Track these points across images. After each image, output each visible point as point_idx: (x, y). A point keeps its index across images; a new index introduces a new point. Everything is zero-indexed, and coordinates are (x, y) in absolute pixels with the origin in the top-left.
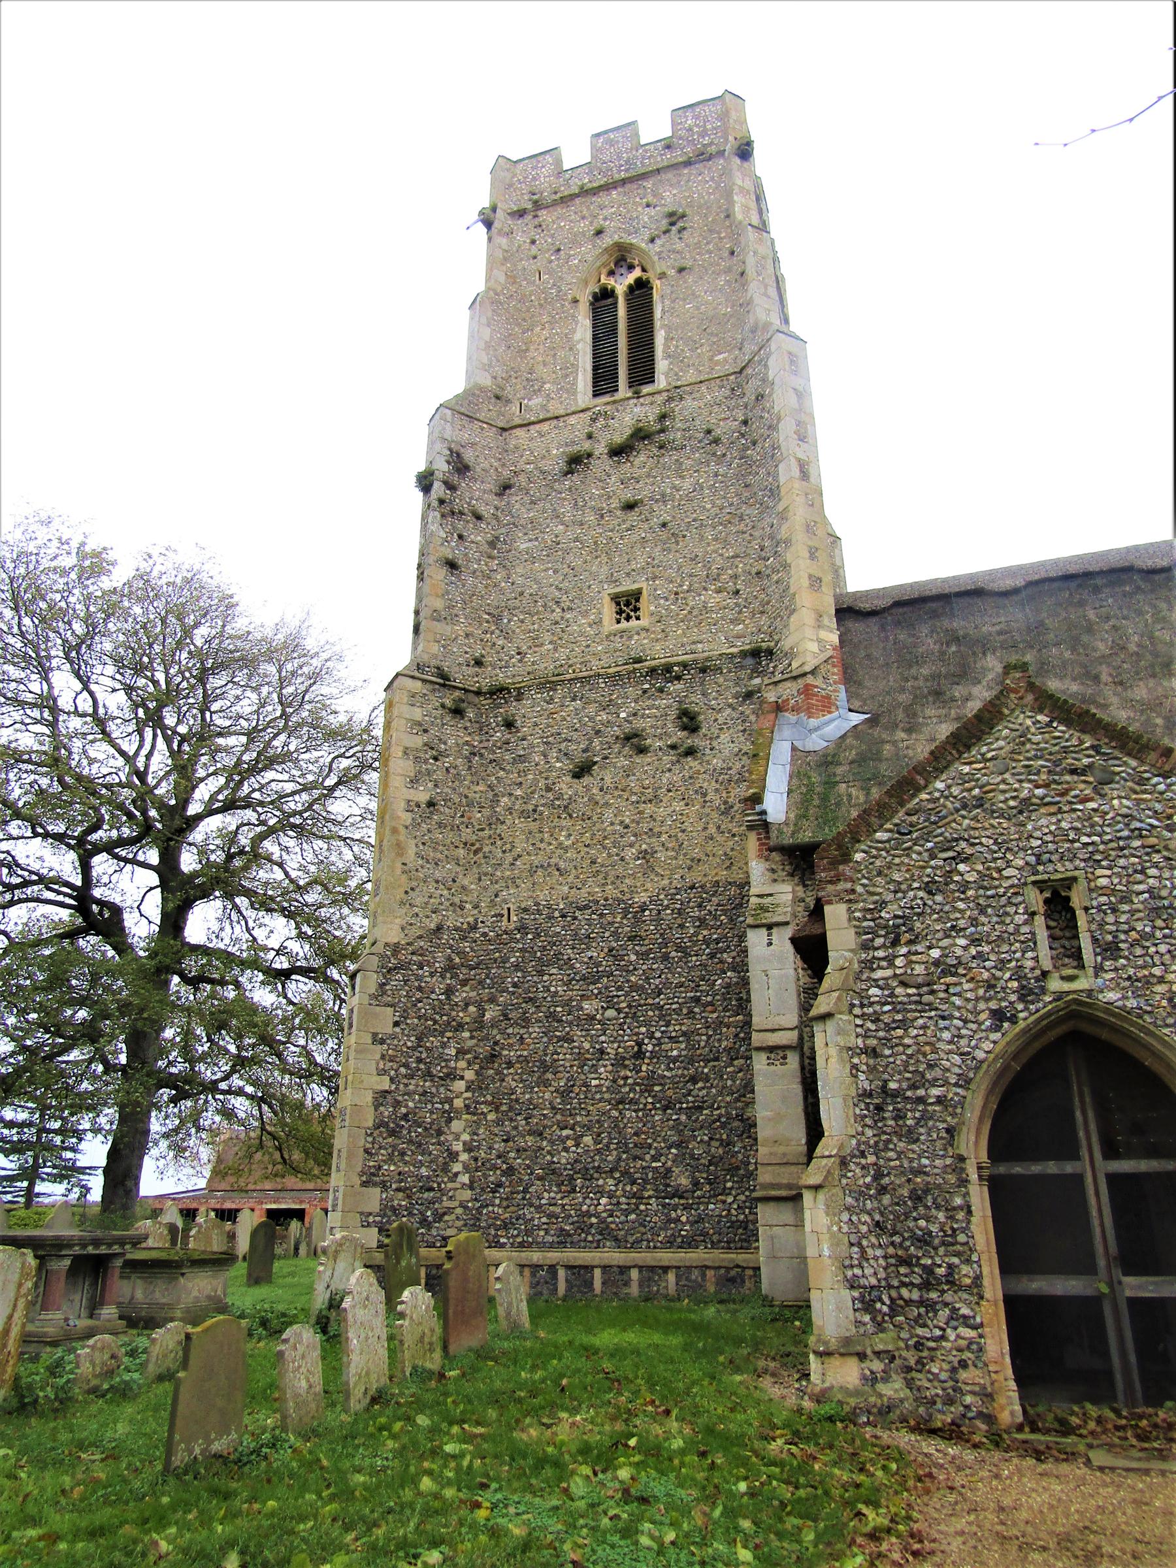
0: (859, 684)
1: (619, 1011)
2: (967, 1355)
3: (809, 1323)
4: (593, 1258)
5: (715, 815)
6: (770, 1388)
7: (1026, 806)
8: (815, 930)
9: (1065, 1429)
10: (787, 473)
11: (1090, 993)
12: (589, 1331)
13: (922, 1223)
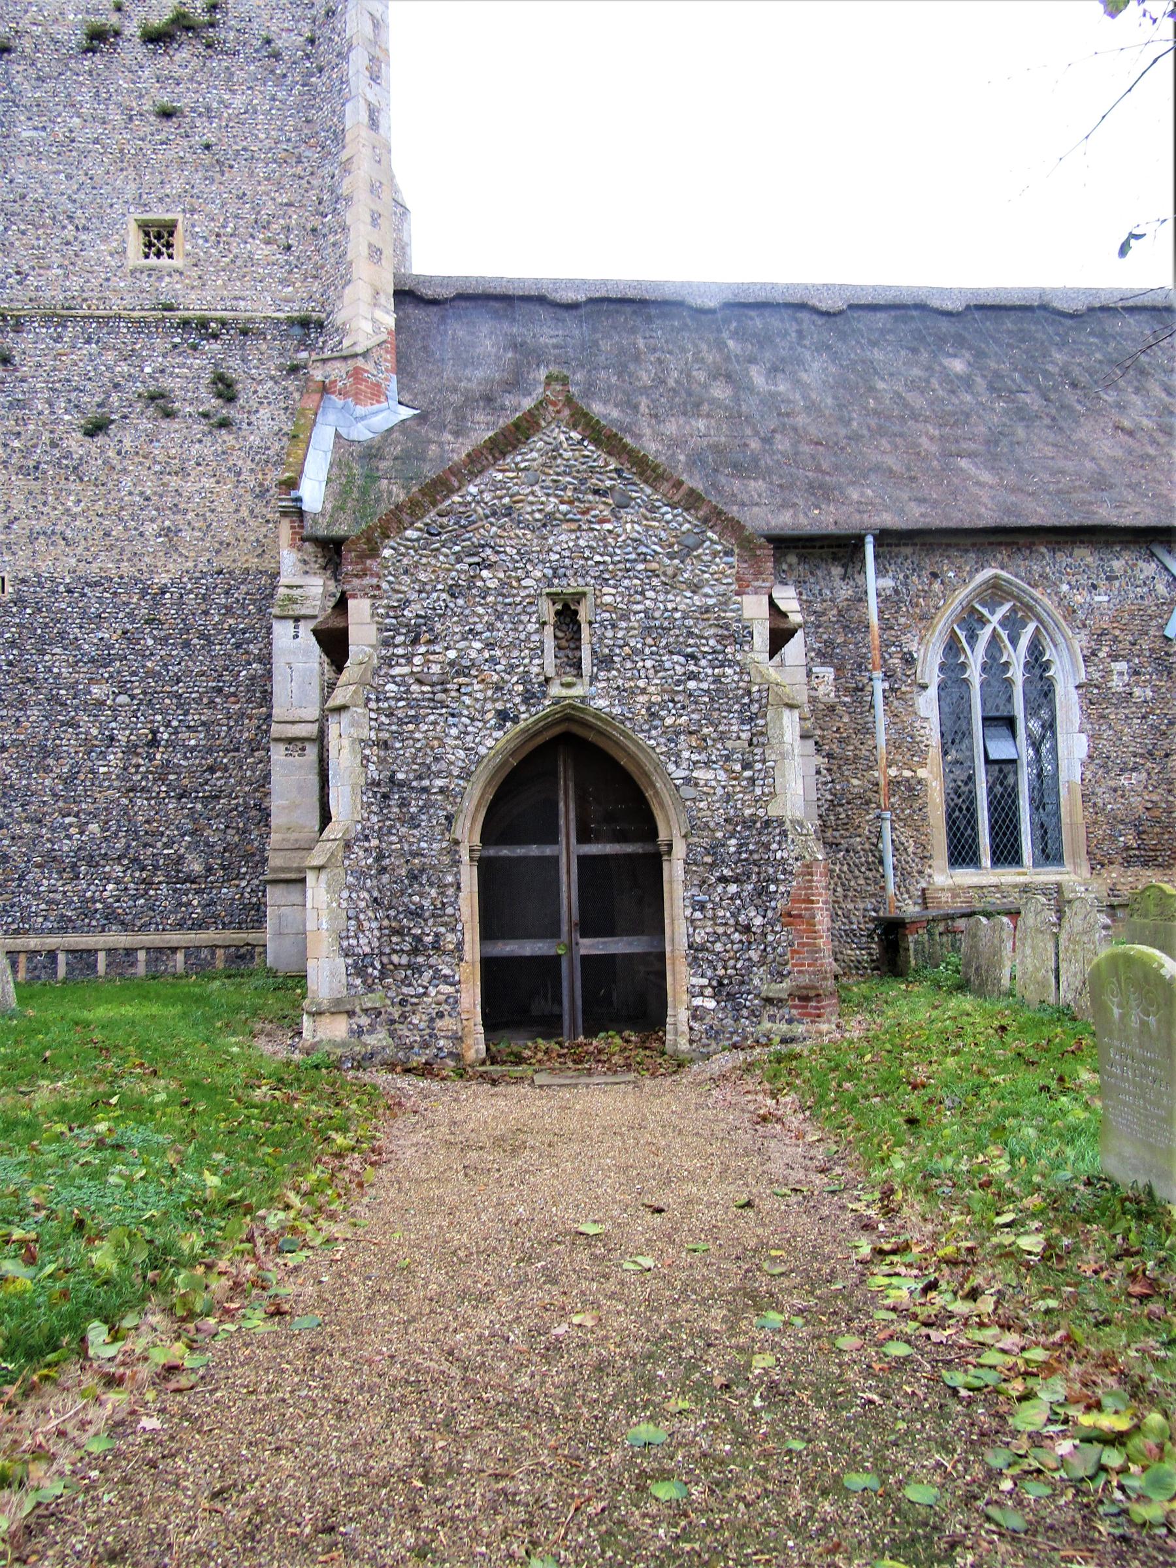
0: (413, 377)
1: (132, 697)
2: (445, 1007)
3: (304, 987)
4: (96, 942)
5: (249, 497)
6: (264, 1046)
7: (550, 520)
8: (337, 623)
9: (519, 1060)
10: (355, 116)
11: (583, 699)
12: (84, 1007)
13: (416, 898)
